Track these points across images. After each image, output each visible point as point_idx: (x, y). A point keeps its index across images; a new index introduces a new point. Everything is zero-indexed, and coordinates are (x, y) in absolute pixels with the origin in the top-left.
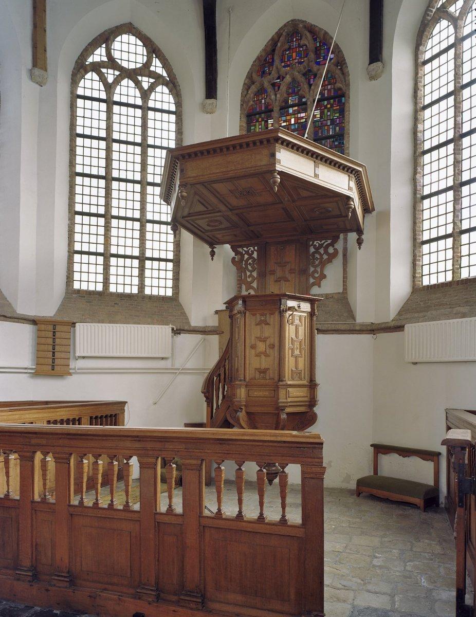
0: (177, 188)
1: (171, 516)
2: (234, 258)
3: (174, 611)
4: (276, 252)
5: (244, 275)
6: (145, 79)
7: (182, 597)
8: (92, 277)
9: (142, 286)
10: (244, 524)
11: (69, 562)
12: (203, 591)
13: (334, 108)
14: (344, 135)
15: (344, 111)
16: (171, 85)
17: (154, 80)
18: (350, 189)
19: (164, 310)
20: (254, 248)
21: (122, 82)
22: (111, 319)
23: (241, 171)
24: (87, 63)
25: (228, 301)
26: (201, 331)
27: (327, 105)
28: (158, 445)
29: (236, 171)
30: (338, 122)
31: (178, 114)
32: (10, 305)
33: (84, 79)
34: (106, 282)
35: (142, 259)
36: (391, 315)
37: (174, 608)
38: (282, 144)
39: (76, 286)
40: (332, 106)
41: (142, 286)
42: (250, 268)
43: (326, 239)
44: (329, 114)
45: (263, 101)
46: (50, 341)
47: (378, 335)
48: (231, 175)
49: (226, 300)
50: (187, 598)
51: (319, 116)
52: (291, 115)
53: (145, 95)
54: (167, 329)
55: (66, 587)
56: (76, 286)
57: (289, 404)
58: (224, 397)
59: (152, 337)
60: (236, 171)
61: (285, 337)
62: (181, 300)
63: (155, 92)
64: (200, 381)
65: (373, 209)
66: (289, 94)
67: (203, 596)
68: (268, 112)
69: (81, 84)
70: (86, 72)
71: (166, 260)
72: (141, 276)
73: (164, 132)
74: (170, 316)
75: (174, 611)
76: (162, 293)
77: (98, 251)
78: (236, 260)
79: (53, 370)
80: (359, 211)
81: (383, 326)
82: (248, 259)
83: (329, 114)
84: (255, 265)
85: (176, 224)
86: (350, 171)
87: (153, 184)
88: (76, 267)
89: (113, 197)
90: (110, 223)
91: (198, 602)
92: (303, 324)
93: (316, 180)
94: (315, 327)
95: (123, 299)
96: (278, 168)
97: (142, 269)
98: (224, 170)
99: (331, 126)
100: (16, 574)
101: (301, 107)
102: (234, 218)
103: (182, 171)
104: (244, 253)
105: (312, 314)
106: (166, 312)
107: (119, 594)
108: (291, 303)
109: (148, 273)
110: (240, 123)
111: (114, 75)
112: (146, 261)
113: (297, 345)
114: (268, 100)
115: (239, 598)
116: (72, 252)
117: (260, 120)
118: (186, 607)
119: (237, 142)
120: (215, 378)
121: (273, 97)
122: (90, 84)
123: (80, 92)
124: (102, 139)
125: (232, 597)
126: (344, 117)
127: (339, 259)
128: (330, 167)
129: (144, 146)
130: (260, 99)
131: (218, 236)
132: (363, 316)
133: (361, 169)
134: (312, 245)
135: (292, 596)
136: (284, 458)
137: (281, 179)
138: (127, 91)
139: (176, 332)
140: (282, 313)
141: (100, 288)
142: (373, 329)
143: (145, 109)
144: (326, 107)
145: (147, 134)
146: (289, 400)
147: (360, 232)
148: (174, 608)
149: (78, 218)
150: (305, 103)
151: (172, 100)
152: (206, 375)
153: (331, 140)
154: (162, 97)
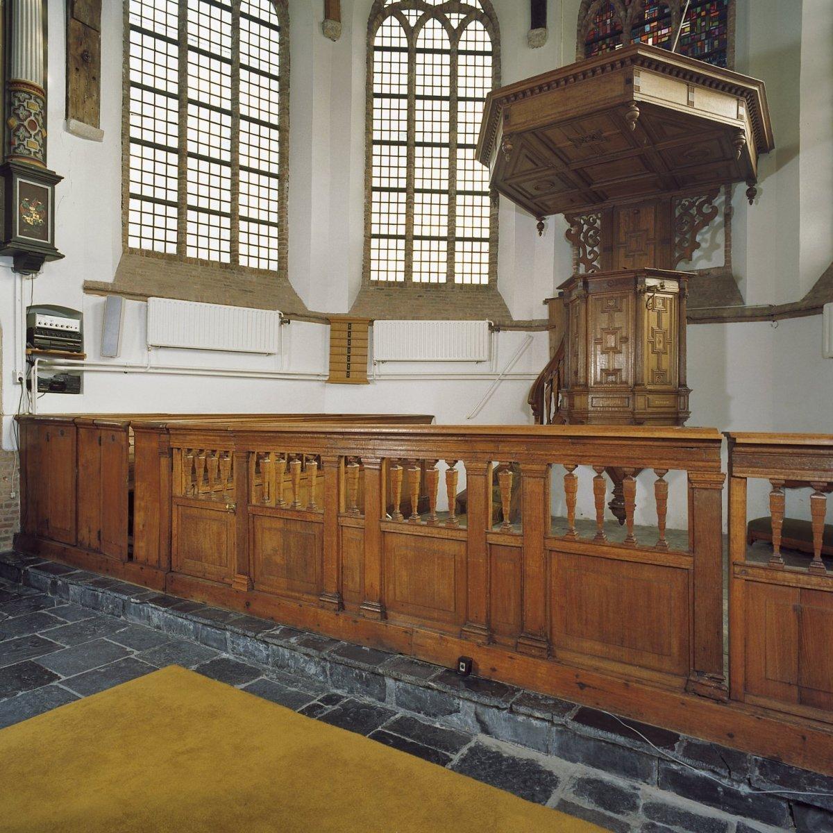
0: (499, 141)
1: (506, 536)
2: (568, 232)
3: (511, 658)
4: (627, 219)
5: (583, 251)
6: (454, 15)
7: (521, 640)
8: (392, 266)
9: (451, 274)
10: (605, 548)
11: (381, 589)
12: (548, 636)
13: (712, 15)
14: (727, 51)
15: (726, 18)
16: (486, 19)
17: (465, 16)
18: (739, 117)
19: (482, 303)
20: (597, 215)
21: (426, 24)
22: (415, 315)
23: (584, 108)
24: (385, 6)
25: (563, 284)
26: (526, 327)
27: (700, 13)
28: (490, 447)
29: (578, 109)
30: (717, 33)
31: (495, 54)
32: (300, 301)
33: (383, 26)
34: (408, 271)
35: (451, 239)
36: (798, 294)
37: (510, 654)
38: (642, 65)
39: (374, 276)
40: (708, 12)
41: (451, 274)
42: (590, 241)
43: (699, 195)
44: (703, 24)
45: (608, 21)
46: (345, 343)
47: (780, 321)
48: (571, 115)
49: (560, 283)
50: (526, 642)
51: (688, 29)
52: (648, 33)
53: (455, 35)
54: (484, 324)
55: (377, 619)
56: (374, 276)
57: (648, 416)
58: (557, 409)
59: (466, 335)
60: (578, 109)
61: (643, 327)
62: (500, 288)
63: (467, 30)
64: (527, 386)
65: (772, 147)
66: (644, 7)
67: (550, 642)
68: (616, 34)
69: (379, 33)
70: (385, 18)
71: (481, 240)
72: (451, 261)
73: (477, 78)
74: (486, 308)
75: (511, 658)
76: (476, 281)
77: (442, 142)
78: (572, 232)
79: (348, 377)
80: (751, 149)
81: (787, 309)
82: (588, 231)
83: (703, 24)
84: (598, 238)
85: (497, 189)
86: (739, 92)
87: (465, 146)
88: (374, 254)
89: (416, 166)
90: (413, 198)
91: (543, 648)
92: (669, 310)
93: (690, 109)
94: (684, 315)
95: (429, 291)
96: (637, 97)
97: (451, 252)
98: (560, 110)
99: (706, 41)
100: (321, 600)
101: (661, 21)
102: (572, 176)
103: (506, 117)
104: (582, 222)
105: (680, 296)
106: (481, 305)
107: (442, 632)
108: (651, 282)
109: (458, 257)
110: (577, 55)
111: (417, 16)
112: (457, 243)
113: (659, 337)
114: (615, 19)
115: (598, 647)
116: (369, 236)
117: (604, 46)
118: (526, 654)
119: (580, 71)
120: (546, 385)
121: (622, 13)
122: (390, 32)
123: (377, 42)
124: (403, 97)
125: (587, 645)
126: (726, 25)
127: (719, 219)
128: (711, 91)
129: (453, 99)
130: (604, 19)
131: (549, 203)
132: (753, 296)
133: (756, 89)
134: (680, 204)
135: (675, 650)
136: (662, 462)
137: (640, 112)
138: (433, 34)
139: (494, 328)
140: (638, 295)
141: (401, 278)
142: (771, 314)
143: (454, 53)
144: (699, 15)
145: (457, 84)
146: (650, 410)
147: (751, 179)
148: (510, 654)
149: (376, 195)
150: (669, 15)
151: (488, 38)
152: (532, 382)
153: (709, 57)
154: (477, 36)
